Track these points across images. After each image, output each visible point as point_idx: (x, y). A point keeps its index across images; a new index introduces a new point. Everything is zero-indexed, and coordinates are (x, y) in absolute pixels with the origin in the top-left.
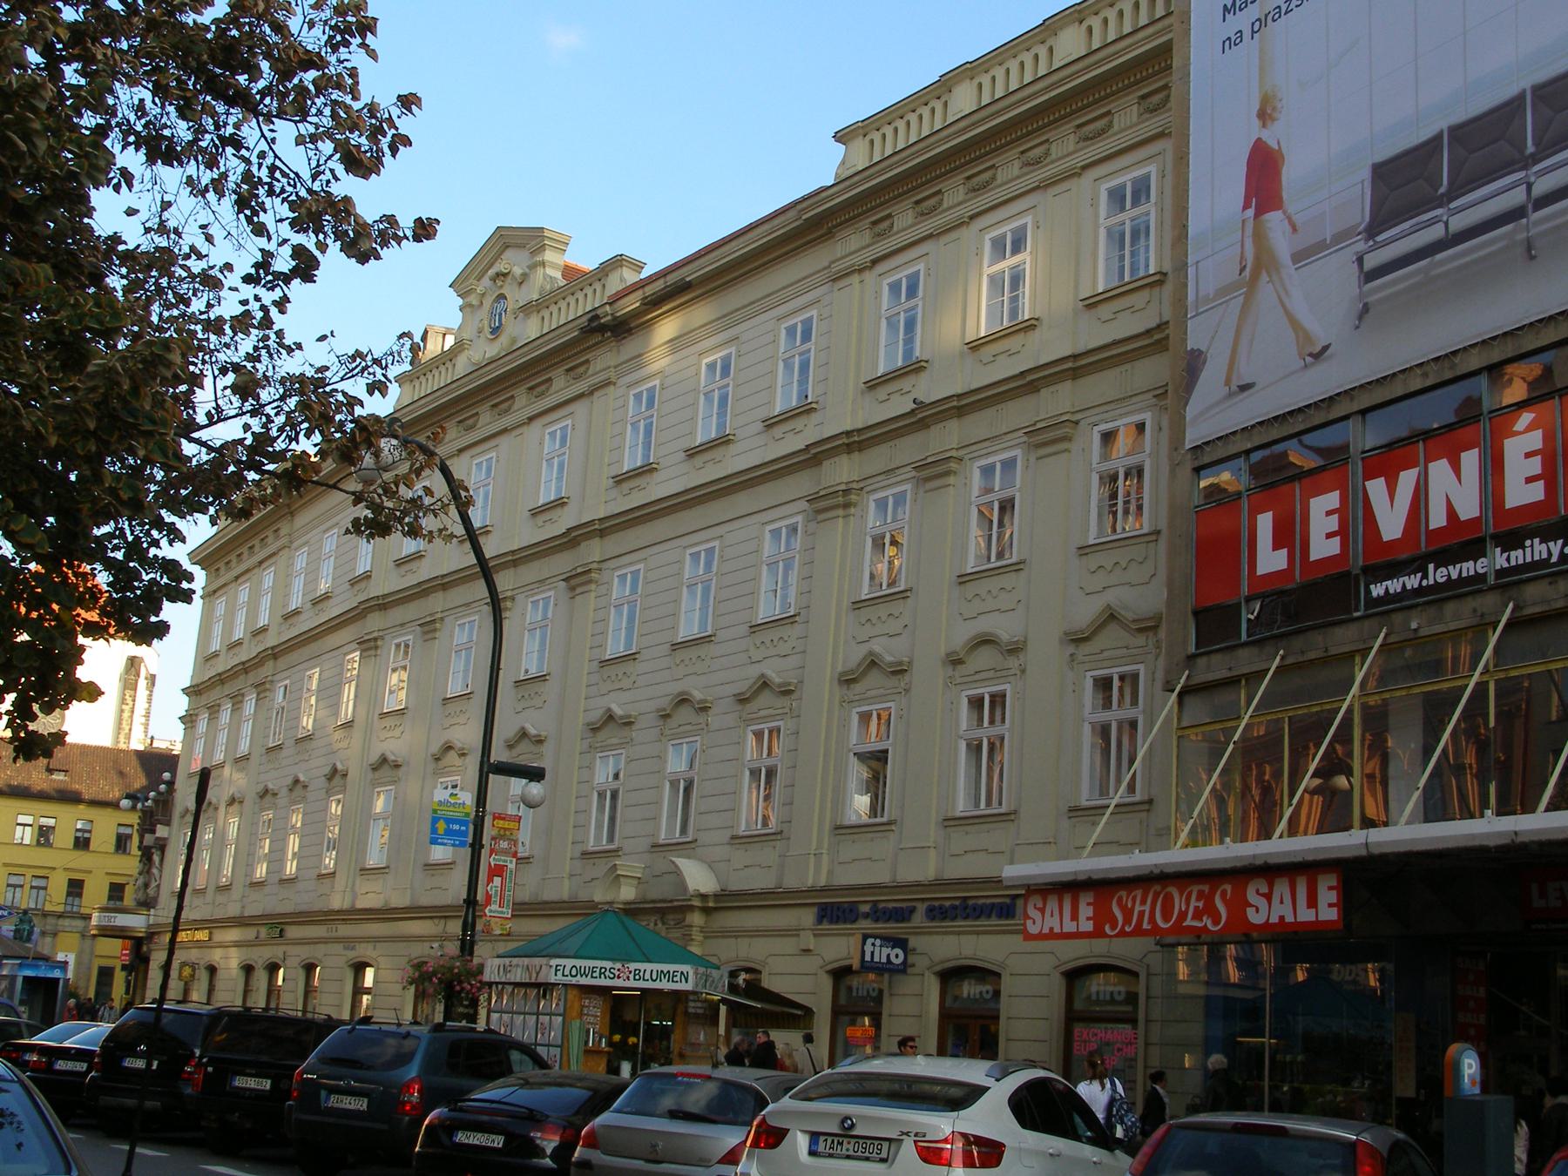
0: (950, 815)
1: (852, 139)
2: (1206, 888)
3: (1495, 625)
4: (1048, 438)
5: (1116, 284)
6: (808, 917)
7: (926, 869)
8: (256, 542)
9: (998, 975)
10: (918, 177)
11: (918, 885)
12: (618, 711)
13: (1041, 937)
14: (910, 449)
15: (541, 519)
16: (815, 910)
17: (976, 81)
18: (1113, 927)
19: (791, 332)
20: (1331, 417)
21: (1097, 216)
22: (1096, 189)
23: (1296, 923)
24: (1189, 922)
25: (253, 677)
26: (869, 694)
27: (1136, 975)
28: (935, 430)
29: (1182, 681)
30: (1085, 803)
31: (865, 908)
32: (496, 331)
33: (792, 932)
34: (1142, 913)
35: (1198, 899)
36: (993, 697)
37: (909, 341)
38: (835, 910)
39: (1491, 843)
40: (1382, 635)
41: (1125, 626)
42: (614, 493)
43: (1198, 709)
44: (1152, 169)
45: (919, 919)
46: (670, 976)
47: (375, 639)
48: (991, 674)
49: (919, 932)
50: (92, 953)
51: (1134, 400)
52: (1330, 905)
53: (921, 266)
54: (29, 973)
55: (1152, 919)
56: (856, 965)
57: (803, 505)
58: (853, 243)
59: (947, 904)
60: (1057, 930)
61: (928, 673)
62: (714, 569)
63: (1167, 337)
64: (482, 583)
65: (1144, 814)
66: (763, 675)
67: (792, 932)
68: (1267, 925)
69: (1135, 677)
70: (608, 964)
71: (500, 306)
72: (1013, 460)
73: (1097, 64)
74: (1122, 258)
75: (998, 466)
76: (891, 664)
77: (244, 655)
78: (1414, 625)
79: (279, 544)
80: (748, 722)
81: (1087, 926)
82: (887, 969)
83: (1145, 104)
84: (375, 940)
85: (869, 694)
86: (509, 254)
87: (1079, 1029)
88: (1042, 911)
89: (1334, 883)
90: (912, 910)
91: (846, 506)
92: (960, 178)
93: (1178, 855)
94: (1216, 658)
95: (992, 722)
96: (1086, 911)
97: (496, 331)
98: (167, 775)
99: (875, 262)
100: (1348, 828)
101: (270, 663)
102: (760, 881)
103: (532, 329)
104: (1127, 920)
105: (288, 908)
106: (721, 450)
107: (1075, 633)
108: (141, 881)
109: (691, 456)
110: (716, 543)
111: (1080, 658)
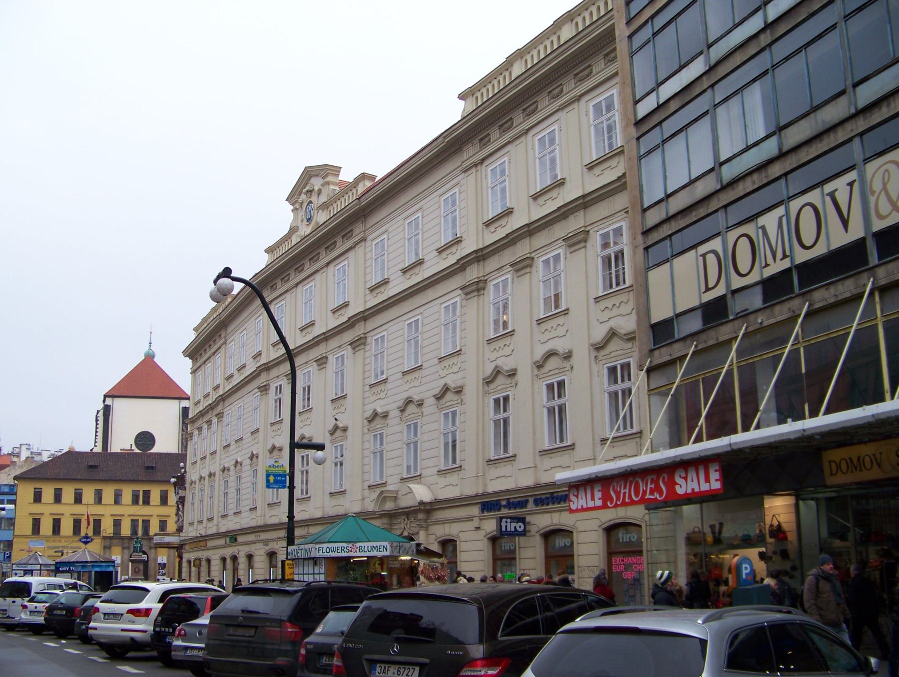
0: (542, 449)
2: (655, 477)
3: (799, 315)
4: (576, 241)
6: (475, 511)
7: (527, 481)
8: (212, 343)
10: (502, 110)
11: (528, 488)
12: (380, 410)
13: (577, 511)
15: (408, 275)
18: (611, 503)
20: (709, 211)
21: (534, 154)
22: (588, 106)
23: (700, 492)
24: (647, 496)
25: (216, 412)
27: (640, 526)
30: (492, 458)
31: (504, 503)
32: (309, 220)
33: (469, 519)
34: (625, 493)
35: (651, 484)
36: (622, 366)
37: (503, 198)
39: (792, 437)
41: (621, 338)
42: (486, 232)
43: (659, 380)
44: (615, 91)
45: (531, 506)
46: (377, 548)
48: (557, 371)
49: (531, 513)
53: (555, 127)
54: (97, 569)
55: (630, 497)
56: (499, 535)
57: (459, 292)
58: (472, 153)
59: (544, 497)
60: (585, 506)
61: (430, 404)
62: (458, 313)
63: (625, 182)
65: (638, 440)
68: (686, 494)
69: (629, 364)
70: (345, 545)
72: (559, 255)
75: (552, 260)
76: (507, 371)
77: (210, 401)
78: (760, 321)
80: (441, 409)
81: (599, 503)
82: (515, 533)
83: (607, 58)
87: (617, 559)
89: (717, 468)
90: (527, 502)
91: (478, 290)
92: (520, 111)
93: (645, 458)
94: (663, 350)
95: (623, 381)
96: (598, 495)
97: (309, 220)
98: (182, 464)
99: (483, 160)
103: (322, 217)
104: (618, 498)
105: (237, 527)
109: (440, 253)
110: (419, 317)
111: (600, 358)
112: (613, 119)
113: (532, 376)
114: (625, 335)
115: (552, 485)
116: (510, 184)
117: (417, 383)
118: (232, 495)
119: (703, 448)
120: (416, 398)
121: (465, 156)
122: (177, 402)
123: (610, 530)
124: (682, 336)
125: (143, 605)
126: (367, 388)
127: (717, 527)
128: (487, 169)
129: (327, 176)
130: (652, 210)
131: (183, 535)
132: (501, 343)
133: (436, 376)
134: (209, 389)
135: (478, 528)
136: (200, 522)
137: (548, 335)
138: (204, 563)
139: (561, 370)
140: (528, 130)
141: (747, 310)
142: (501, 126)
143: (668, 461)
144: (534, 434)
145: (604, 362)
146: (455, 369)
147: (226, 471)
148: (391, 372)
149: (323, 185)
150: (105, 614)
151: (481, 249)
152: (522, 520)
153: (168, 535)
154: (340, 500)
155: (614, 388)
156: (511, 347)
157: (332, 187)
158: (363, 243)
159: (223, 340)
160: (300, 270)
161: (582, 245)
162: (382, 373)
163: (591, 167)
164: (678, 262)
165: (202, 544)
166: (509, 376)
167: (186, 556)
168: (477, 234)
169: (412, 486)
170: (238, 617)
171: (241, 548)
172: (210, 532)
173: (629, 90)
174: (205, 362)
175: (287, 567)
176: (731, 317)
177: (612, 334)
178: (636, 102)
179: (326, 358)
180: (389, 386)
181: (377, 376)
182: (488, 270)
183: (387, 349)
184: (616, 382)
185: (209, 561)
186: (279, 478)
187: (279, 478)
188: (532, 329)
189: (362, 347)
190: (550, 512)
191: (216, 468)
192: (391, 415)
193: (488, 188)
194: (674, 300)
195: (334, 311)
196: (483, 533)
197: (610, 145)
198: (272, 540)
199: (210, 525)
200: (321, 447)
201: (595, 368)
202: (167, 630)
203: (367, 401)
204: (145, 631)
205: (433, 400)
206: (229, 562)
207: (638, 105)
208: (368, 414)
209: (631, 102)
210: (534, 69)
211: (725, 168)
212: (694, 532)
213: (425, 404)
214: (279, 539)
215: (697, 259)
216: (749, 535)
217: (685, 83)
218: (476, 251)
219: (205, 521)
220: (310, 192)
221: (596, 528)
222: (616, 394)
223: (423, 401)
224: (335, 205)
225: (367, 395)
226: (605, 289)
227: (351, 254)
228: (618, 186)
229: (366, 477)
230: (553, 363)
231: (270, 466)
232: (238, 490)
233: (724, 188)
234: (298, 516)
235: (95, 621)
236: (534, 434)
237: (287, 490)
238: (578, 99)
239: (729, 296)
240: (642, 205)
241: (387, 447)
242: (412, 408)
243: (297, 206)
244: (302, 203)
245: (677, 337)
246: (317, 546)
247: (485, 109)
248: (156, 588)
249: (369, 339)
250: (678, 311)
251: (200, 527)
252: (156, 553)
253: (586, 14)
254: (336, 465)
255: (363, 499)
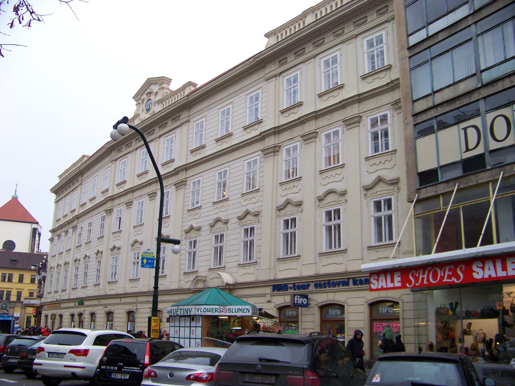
1: (270, 36)
2: (453, 267)
4: (353, 122)
5: (328, 89)
6: (269, 290)
7: (309, 272)
9: (343, 306)
13: (377, 290)
14: (298, 131)
16: (272, 287)
17: (315, 13)
18: (410, 284)
19: (251, 98)
20: (471, 101)
21: (363, 49)
22: (363, 42)
23: (497, 277)
24: (445, 280)
25: (71, 225)
26: (288, 213)
28: (349, 108)
29: (416, 197)
31: (291, 286)
32: (148, 110)
33: (264, 295)
34: (423, 279)
35: (449, 271)
37: (171, 154)
38: (279, 287)
40: (502, 174)
45: (312, 288)
46: (242, 310)
47: (110, 209)
48: (334, 203)
49: (312, 293)
50: (25, 312)
51: (382, 107)
52: (399, 282)
55: (428, 280)
57: (260, 152)
58: (272, 69)
60: (385, 287)
61: (234, 223)
64: (159, 184)
66: (191, 226)
67: (264, 295)
70: (218, 307)
71: (149, 103)
73: (329, 18)
74: (329, 81)
75: (332, 134)
79: (78, 184)
81: (399, 285)
82: (302, 305)
84: (114, 304)
85: (288, 213)
86: (152, 87)
87: (376, 324)
88: (378, 280)
90: (308, 285)
91: (274, 152)
92: (352, 22)
95: (291, 227)
97: (148, 110)
99: (281, 73)
100: (461, 248)
101: (76, 220)
102: (251, 278)
103: (157, 108)
106: (228, 138)
107: (367, 186)
108: (38, 290)
109: (245, 129)
110: (227, 168)
111: (369, 195)
112: (296, 87)
113: (315, 206)
114: (389, 181)
115: (359, 272)
116: (301, 89)
117: (224, 209)
118: (81, 275)
119: (507, 247)
120: (139, 240)
121: (268, 70)
122: (30, 224)
123: (373, 305)
124: (445, 180)
125: (82, 347)
126: (186, 212)
127: (454, 304)
128: (283, 80)
129: (163, 83)
130: (420, 101)
131: (43, 300)
132: (251, 196)
133: (239, 205)
134: (67, 212)
135: (269, 302)
136: (56, 292)
137: (327, 181)
138: (57, 317)
139: (337, 203)
140: (316, 55)
141: (502, 163)
142: (280, 61)
143: (470, 256)
144: (315, 242)
145: (371, 198)
146: (254, 201)
147: (77, 262)
148: (203, 202)
149: (159, 89)
150: (49, 353)
151: (279, 127)
152: (306, 297)
153: (33, 299)
154: (113, 287)
155: (379, 214)
156: (299, 188)
157: (165, 90)
158: (187, 124)
159: (80, 182)
160: (120, 151)
161: (357, 124)
162: (197, 203)
163: (321, 96)
164: (443, 134)
165: (57, 305)
166: (296, 205)
167: (44, 313)
168: (275, 118)
169: (220, 273)
170: (257, 365)
171: (86, 309)
172: (63, 298)
173: (403, 28)
174: (65, 196)
175: (152, 321)
176: (488, 168)
177: (380, 180)
178: (409, 36)
179: (132, 202)
180: (202, 211)
181: (193, 205)
182: (281, 141)
183: (229, 178)
184: (288, 228)
185: (61, 316)
186: (150, 261)
187: (150, 261)
188: (315, 176)
189: (183, 186)
190: (327, 292)
191: (70, 259)
192: (203, 229)
193: (283, 90)
194: (438, 157)
195: (139, 176)
196: (273, 305)
197: (294, 101)
198: (110, 304)
199: (63, 294)
200: (177, 242)
201: (364, 202)
202: (112, 368)
203: (185, 220)
204: (84, 368)
205: (236, 220)
206: (76, 318)
207: (410, 37)
208: (187, 228)
209: (406, 35)
210: (347, 6)
211: (484, 74)
212: (441, 308)
213: (230, 223)
214: (147, 302)
215: (459, 131)
216: (469, 311)
217: (451, 22)
218: (274, 128)
219: (60, 291)
220: (150, 93)
221: (272, 307)
222: (287, 234)
223: (228, 220)
224: (167, 101)
225: (185, 216)
226: (326, 166)
227: (178, 131)
228: (393, 86)
229: (182, 267)
230: (219, 225)
231: (144, 253)
232: (86, 274)
233: (484, 86)
234: (161, 287)
235: (40, 358)
236: (315, 242)
237: (154, 269)
238: (356, 36)
239: (487, 154)
240: (412, 98)
241: (89, 271)
242: (137, 245)
243: (140, 101)
244: (144, 100)
245: (440, 180)
246: (197, 307)
247: (287, 41)
248: (91, 334)
249: (188, 182)
250: (441, 164)
251: (56, 295)
252: (13, 311)
253: (323, 10)
254: (134, 263)
255: (180, 281)
